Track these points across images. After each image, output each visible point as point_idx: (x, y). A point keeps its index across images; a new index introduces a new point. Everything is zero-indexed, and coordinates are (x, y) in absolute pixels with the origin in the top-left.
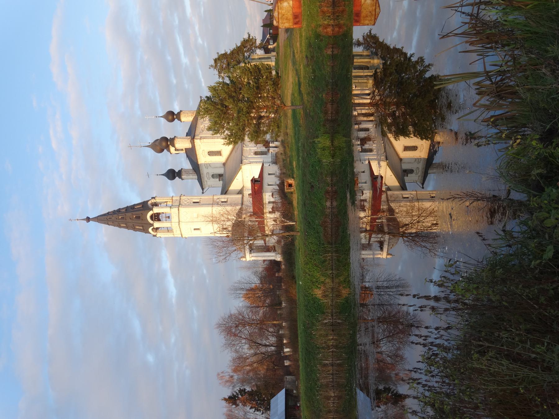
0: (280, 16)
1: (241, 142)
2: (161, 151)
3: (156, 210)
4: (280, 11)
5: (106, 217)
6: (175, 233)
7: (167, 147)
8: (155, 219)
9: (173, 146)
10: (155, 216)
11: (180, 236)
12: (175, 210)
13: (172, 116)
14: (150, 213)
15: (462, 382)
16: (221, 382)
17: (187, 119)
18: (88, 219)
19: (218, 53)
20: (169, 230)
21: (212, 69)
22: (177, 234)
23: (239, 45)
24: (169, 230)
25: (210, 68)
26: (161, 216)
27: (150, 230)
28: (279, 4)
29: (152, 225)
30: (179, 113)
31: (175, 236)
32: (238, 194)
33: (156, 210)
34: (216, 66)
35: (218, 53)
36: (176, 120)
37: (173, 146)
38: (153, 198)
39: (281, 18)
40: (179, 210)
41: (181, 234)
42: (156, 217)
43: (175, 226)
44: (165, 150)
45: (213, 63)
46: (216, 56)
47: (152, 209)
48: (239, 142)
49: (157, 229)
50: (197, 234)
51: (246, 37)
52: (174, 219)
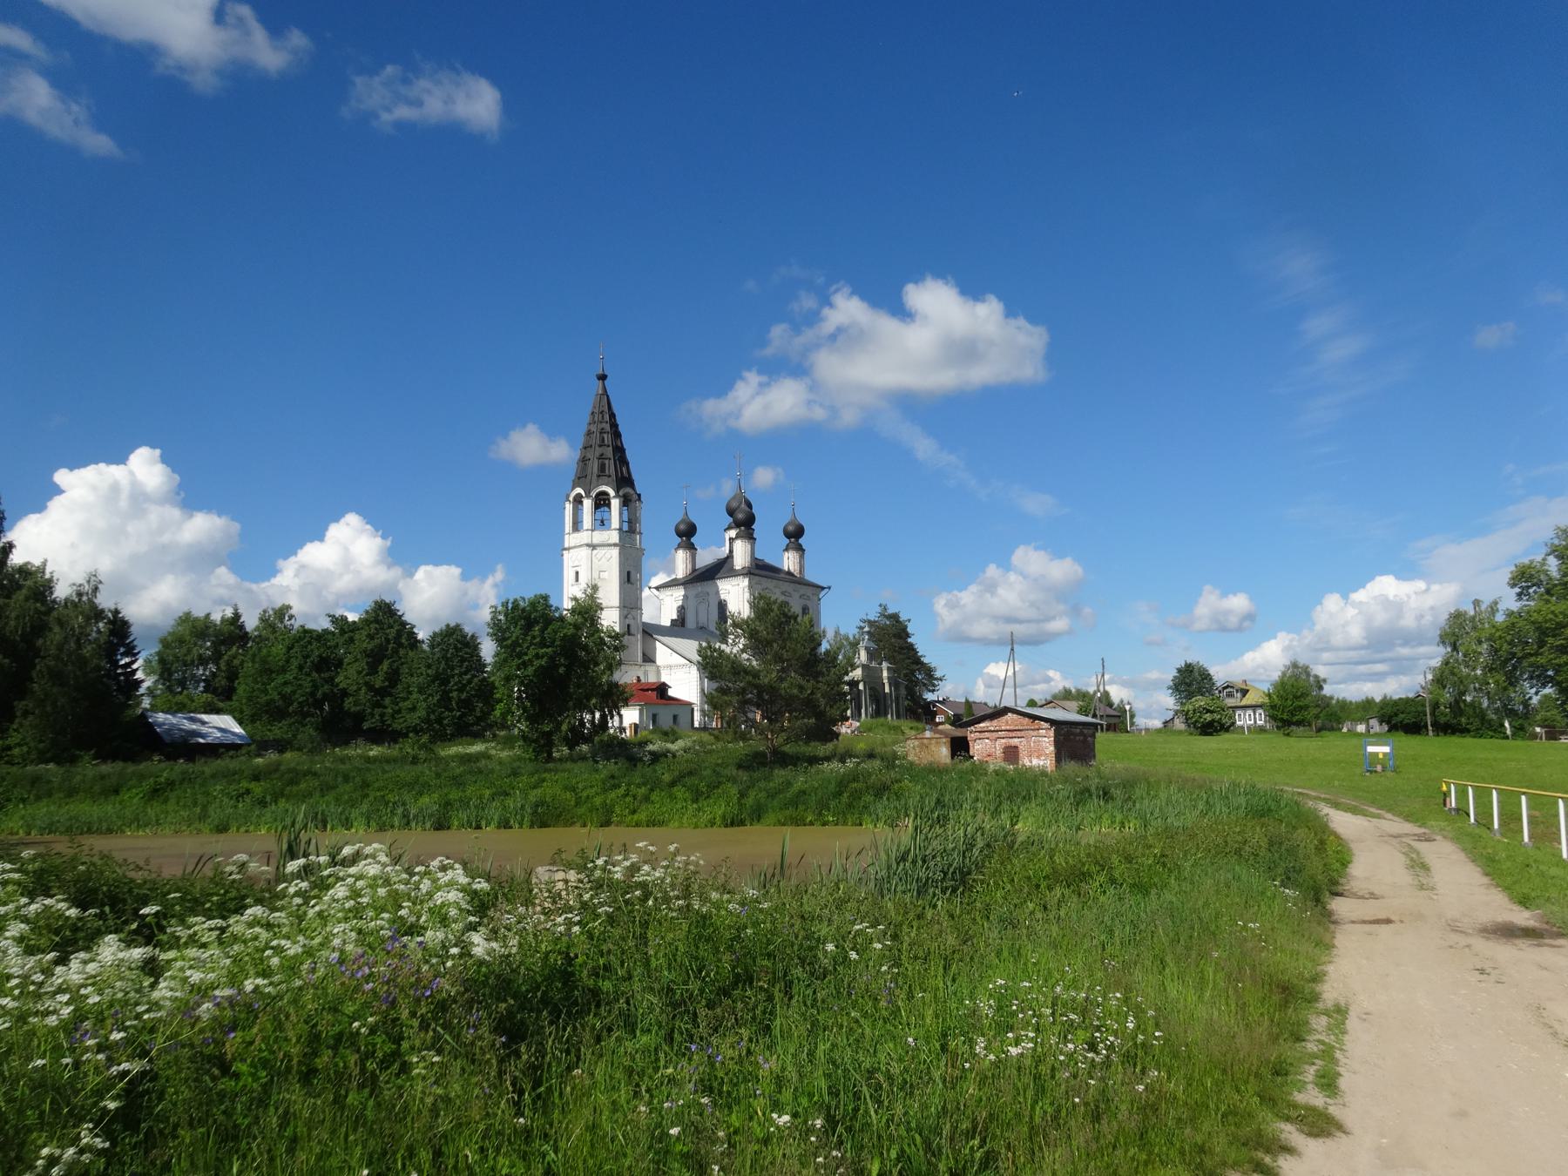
0: (925, 741)
1: (699, 662)
2: (731, 512)
3: (615, 503)
4: (933, 741)
5: (606, 409)
6: (572, 536)
7: (737, 524)
8: (600, 500)
9: (738, 537)
10: (604, 500)
11: (566, 545)
12: (614, 537)
13: (795, 534)
14: (612, 493)
15: (246, 1094)
16: (1483, 607)
17: (789, 562)
18: (603, 377)
19: (909, 621)
20: (577, 526)
21: (879, 610)
22: (571, 539)
23: (925, 660)
24: (577, 526)
25: (880, 605)
26: (606, 509)
27: (579, 490)
28: (944, 740)
29: (588, 496)
30: (800, 549)
31: (566, 537)
32: (644, 654)
33: (615, 503)
34: (885, 616)
35: (909, 621)
36: (788, 541)
37: (738, 537)
38: (639, 495)
39: (923, 744)
40: (610, 545)
41: (568, 549)
42: (601, 502)
43: (584, 537)
44: (731, 520)
45: (891, 611)
46: (903, 617)
47: (617, 496)
48: (700, 659)
49: (581, 503)
50: (568, 575)
51: (938, 674)
52: (599, 537)
